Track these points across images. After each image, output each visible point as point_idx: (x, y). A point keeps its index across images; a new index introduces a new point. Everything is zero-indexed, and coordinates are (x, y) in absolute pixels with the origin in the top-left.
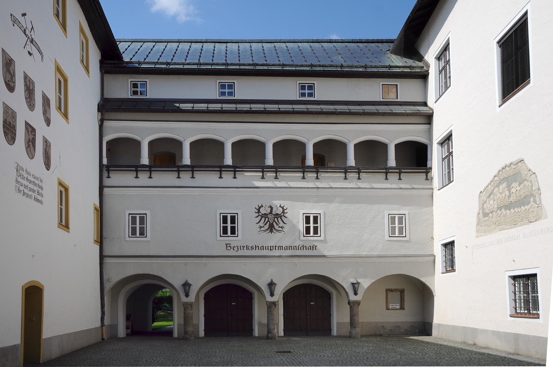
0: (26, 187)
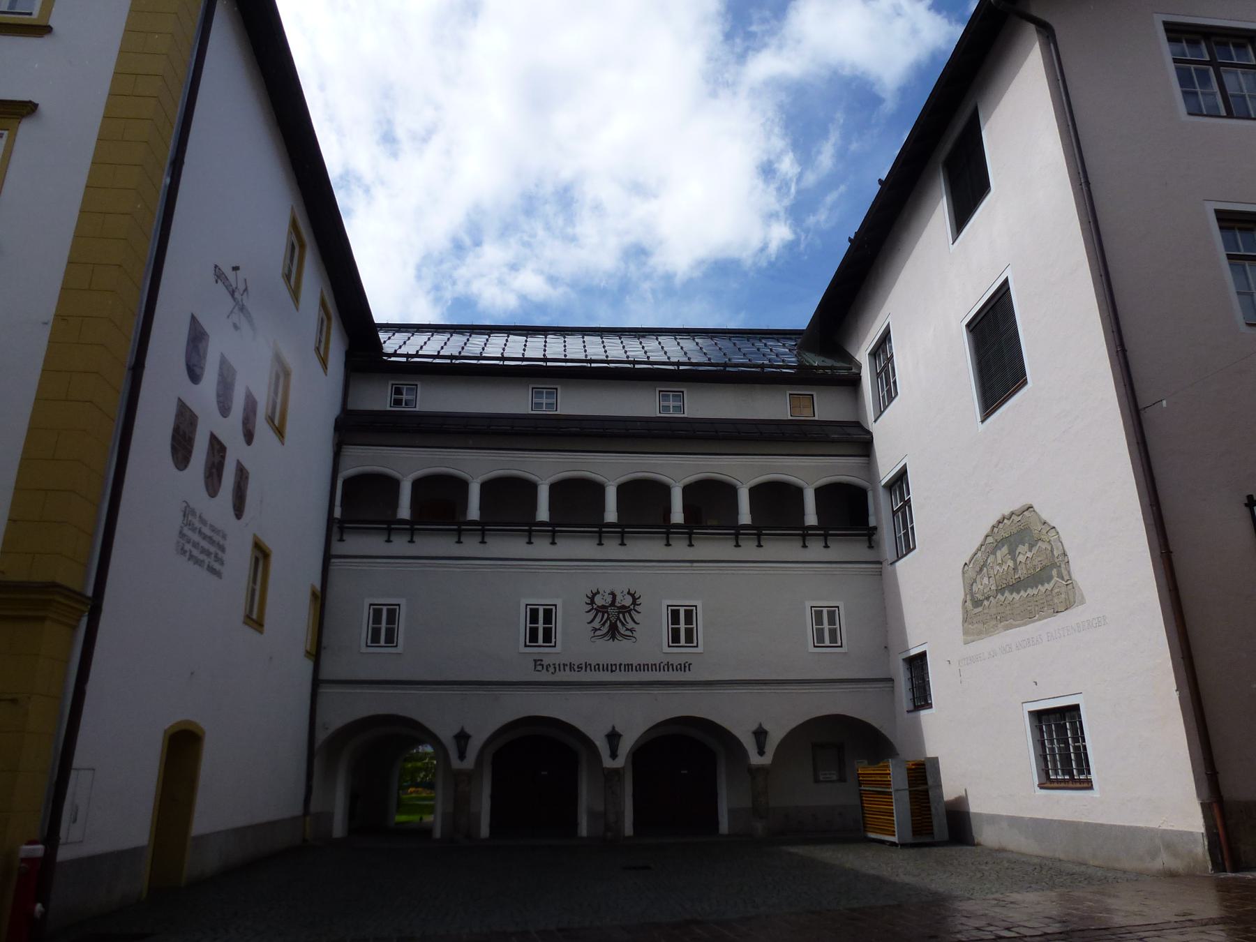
0: (195, 545)
